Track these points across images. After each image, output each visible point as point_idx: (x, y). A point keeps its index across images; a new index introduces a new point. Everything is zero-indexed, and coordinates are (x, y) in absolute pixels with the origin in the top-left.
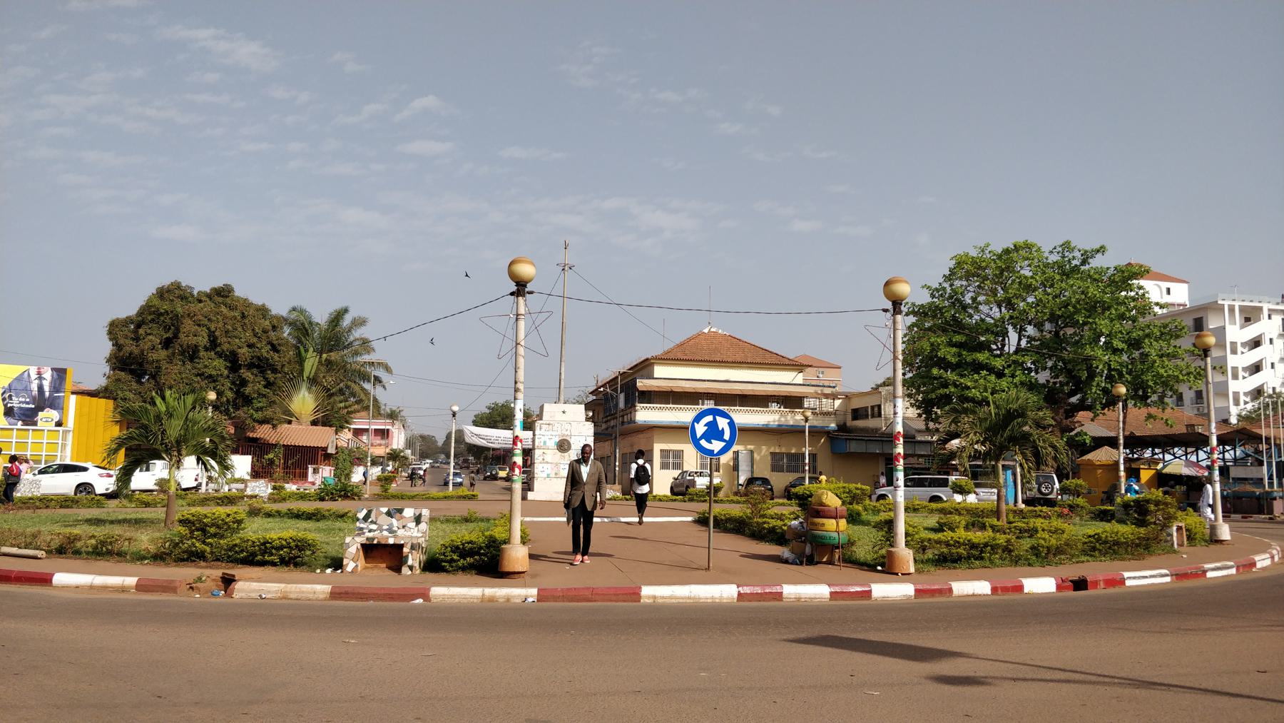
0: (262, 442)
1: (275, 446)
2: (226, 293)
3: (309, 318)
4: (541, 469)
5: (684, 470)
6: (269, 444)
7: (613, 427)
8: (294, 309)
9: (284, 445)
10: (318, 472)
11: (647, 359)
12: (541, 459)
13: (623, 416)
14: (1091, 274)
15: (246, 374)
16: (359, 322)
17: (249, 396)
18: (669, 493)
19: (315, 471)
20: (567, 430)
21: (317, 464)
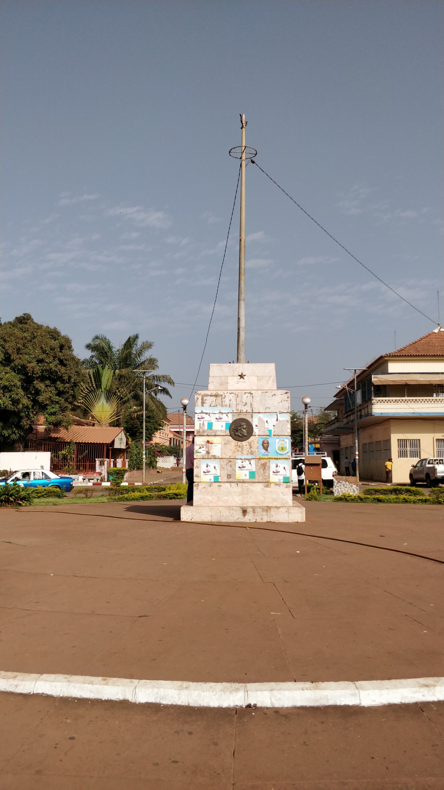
0: (59, 441)
1: (69, 443)
2: (26, 321)
3: (110, 348)
4: (203, 468)
5: (422, 458)
6: (64, 442)
7: (352, 421)
8: (97, 338)
9: (76, 443)
11: (381, 357)
12: (203, 452)
13: (360, 410)
15: (40, 386)
16: (148, 346)
17: (42, 403)
18: (408, 481)
19: (102, 463)
20: (246, 404)
21: (103, 458)
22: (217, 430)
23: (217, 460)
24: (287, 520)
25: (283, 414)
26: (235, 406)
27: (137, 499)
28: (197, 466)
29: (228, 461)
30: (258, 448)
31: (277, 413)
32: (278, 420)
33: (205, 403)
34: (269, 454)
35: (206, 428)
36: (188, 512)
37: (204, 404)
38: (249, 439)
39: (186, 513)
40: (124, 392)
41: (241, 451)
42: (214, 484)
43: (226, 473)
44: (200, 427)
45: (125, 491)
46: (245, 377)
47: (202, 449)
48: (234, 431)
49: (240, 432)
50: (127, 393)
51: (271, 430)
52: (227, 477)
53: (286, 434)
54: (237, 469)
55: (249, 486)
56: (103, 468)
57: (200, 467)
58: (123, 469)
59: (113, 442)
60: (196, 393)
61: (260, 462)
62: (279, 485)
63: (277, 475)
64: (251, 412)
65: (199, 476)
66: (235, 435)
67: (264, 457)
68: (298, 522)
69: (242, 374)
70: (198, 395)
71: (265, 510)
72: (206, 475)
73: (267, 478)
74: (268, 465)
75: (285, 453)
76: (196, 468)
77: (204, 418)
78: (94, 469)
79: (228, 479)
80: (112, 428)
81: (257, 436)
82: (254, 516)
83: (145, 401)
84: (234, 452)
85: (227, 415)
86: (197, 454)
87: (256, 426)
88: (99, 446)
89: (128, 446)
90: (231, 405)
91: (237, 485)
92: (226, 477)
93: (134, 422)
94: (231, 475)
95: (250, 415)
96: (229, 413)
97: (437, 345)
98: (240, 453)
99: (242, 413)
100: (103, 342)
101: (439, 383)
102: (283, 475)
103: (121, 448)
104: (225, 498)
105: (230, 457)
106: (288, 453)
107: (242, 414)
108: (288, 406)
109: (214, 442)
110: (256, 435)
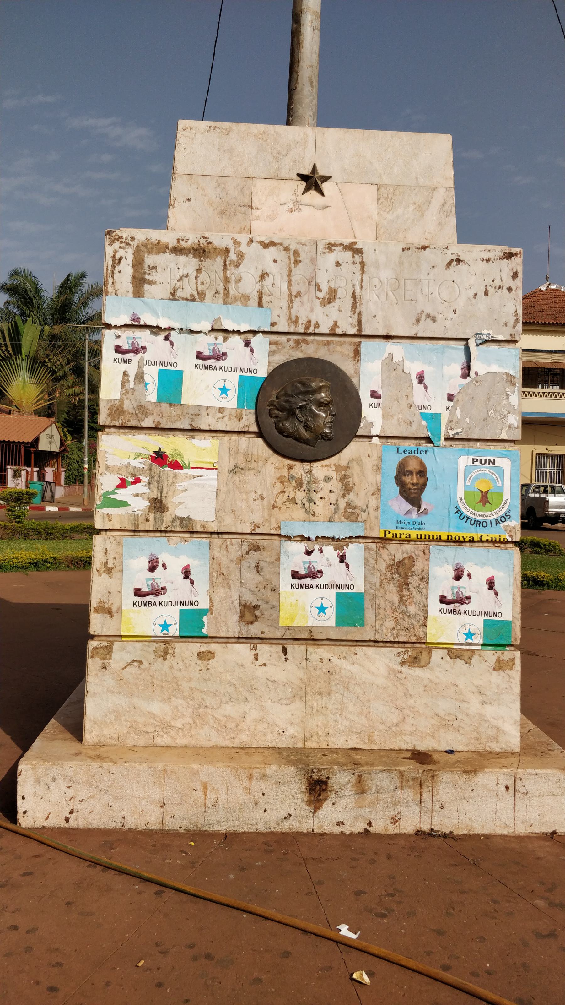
3: (37, 291)
10: (20, 476)
14: (57, 790)
19: (17, 474)
21: (19, 465)
22: (199, 407)
23: (196, 540)
24: (507, 827)
25: (494, 347)
26: (284, 303)
27: (23, 567)
28: (105, 565)
29: (245, 548)
30: (377, 492)
31: (467, 340)
32: (472, 374)
33: (151, 282)
34: (423, 519)
35: (152, 395)
36: (53, 785)
37: (147, 286)
38: (340, 451)
39: (41, 790)
40: (58, 363)
41: (307, 505)
42: (180, 647)
43: (236, 596)
44: (125, 392)
45: (31, 531)
46: (325, 186)
47: (131, 489)
48: (276, 417)
49: (303, 419)
50: (64, 364)
51: (437, 417)
52: (242, 616)
53: (504, 436)
54: (286, 580)
55: (335, 660)
56: (19, 482)
57: (121, 571)
58: (28, 492)
59: (36, 440)
60: (109, 233)
61: (384, 554)
62: (466, 655)
63: (460, 612)
64: (353, 331)
65: (114, 609)
66: (281, 432)
67: (405, 533)
68: (554, 832)
69: (314, 169)
70: (117, 245)
71: (410, 783)
72: (143, 608)
73: (416, 625)
74: (418, 566)
75: (495, 516)
76: (100, 575)
77: (144, 348)
78: (5, 482)
79: (243, 624)
80: (37, 418)
81: (375, 440)
82: (362, 807)
83: (88, 378)
84: (274, 506)
85: (247, 344)
86: (107, 510)
87: (374, 395)
88: (13, 446)
89: (63, 448)
90: (268, 299)
91: (285, 651)
92: (236, 618)
93: (78, 412)
94: (256, 607)
95: (351, 344)
96: (254, 333)
97: (546, 308)
98: (299, 513)
99: (315, 334)
100: (27, 280)
101: (550, 367)
102: (486, 614)
103: (52, 450)
104: (229, 709)
105: (256, 526)
106: (507, 516)
107: (312, 342)
108: (516, 315)
109: (187, 458)
110: (371, 437)
